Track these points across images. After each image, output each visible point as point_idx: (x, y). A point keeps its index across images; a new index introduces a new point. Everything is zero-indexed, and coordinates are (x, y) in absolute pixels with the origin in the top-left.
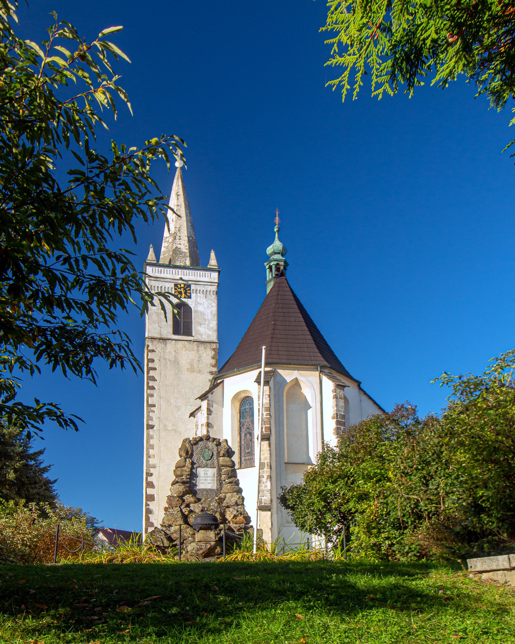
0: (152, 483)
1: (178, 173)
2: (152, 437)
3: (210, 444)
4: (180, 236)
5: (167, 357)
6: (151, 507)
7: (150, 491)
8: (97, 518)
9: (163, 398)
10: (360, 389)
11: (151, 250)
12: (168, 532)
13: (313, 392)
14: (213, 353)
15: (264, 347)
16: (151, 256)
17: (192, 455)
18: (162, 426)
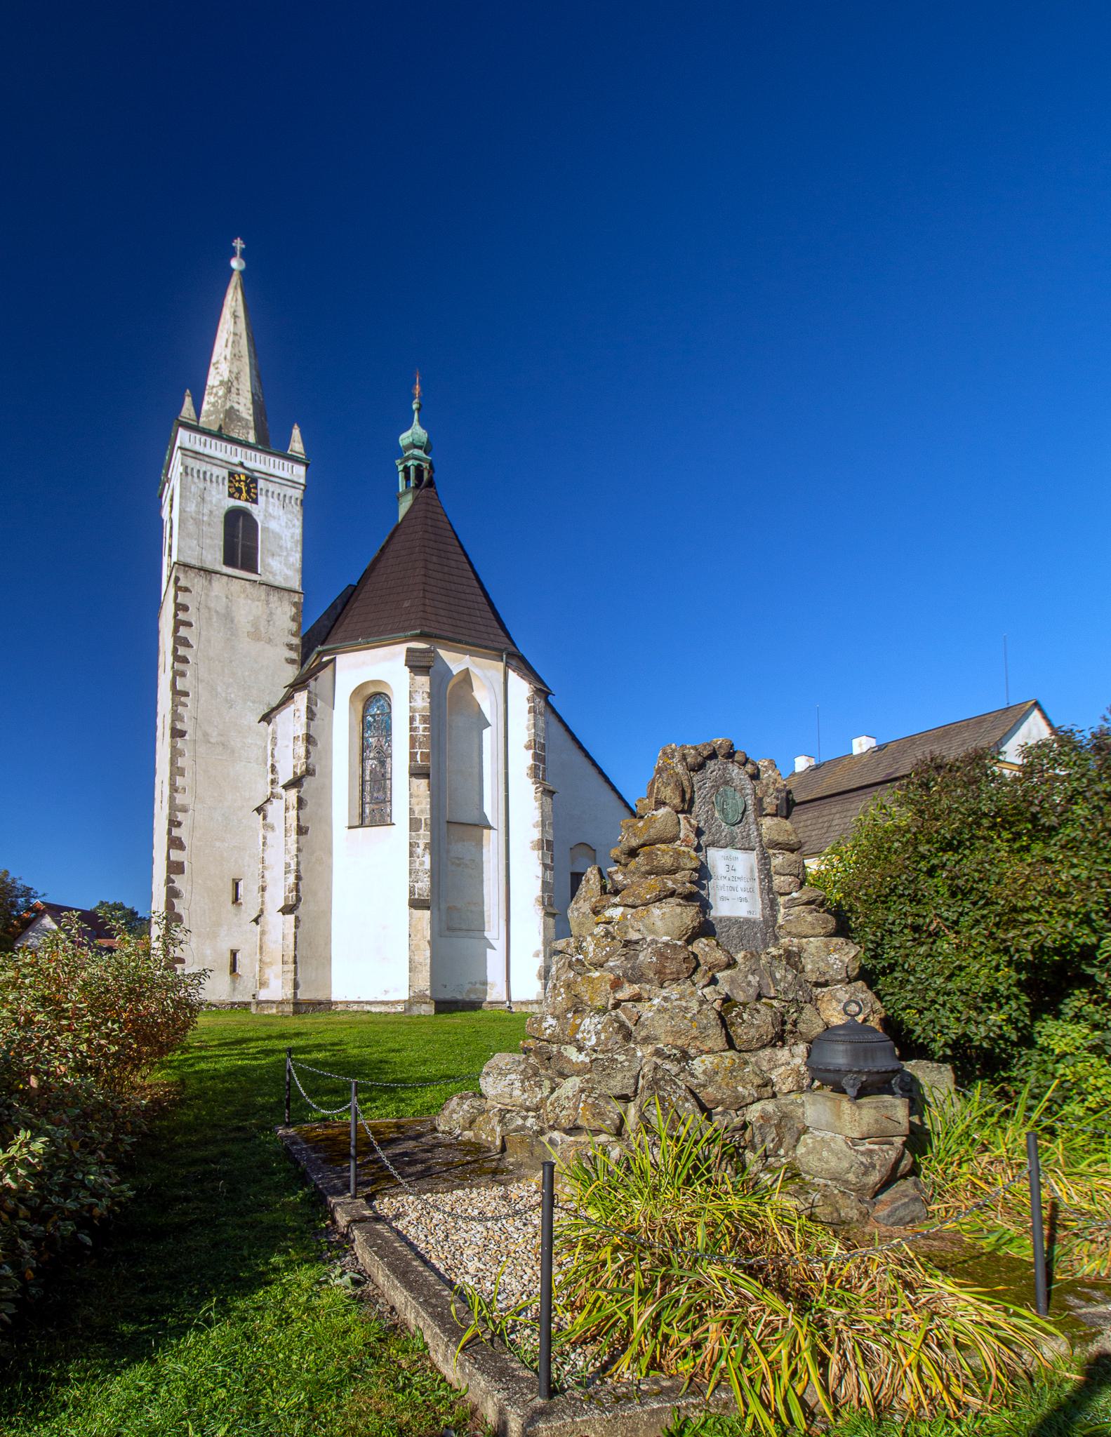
0: (179, 839)
1: (235, 280)
2: (182, 754)
3: (735, 771)
5: (212, 605)
8: (36, 889)
9: (202, 681)
11: (188, 401)
13: (493, 698)
14: (294, 610)
16: (187, 410)
18: (199, 733)
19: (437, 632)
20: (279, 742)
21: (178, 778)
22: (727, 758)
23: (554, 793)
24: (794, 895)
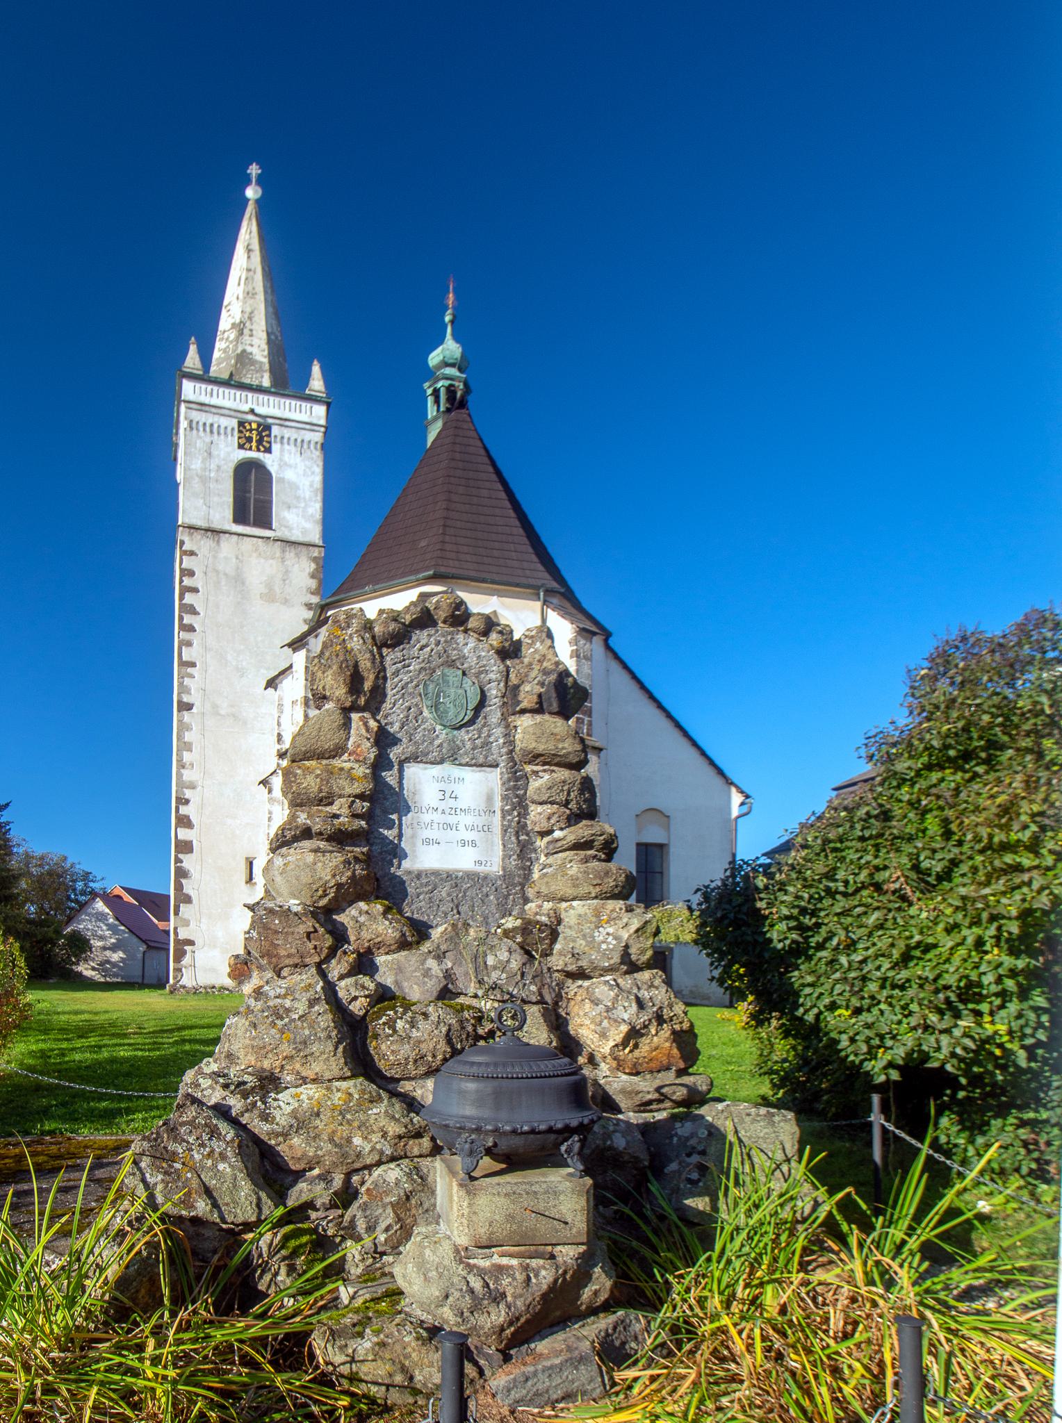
0: (188, 817)
1: (250, 209)
2: (189, 728)
3: (469, 646)
5: (220, 568)
6: (185, 865)
7: (184, 834)
8: (94, 873)
10: (608, 648)
11: (193, 349)
12: (261, 1128)
14: (313, 566)
16: (192, 360)
17: (378, 694)
19: (454, 571)
21: (185, 753)
22: (452, 625)
23: (601, 750)
24: (558, 834)
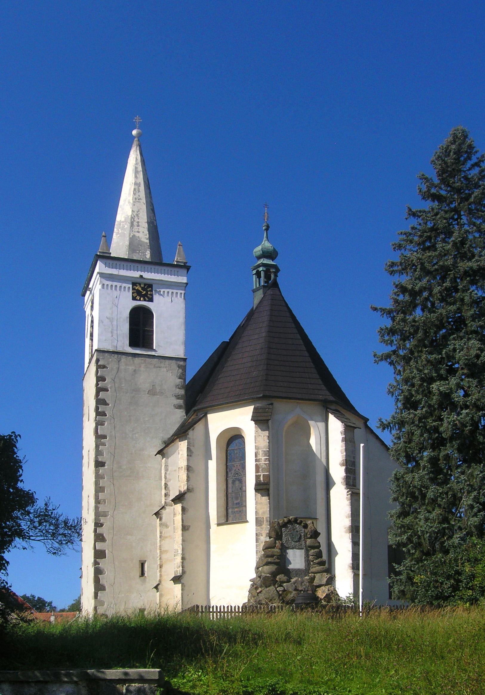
0: (102, 535)
4: (138, 222)
15: (362, 445)
20: (170, 468)
